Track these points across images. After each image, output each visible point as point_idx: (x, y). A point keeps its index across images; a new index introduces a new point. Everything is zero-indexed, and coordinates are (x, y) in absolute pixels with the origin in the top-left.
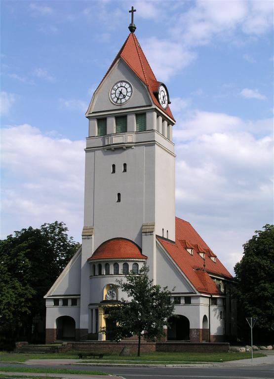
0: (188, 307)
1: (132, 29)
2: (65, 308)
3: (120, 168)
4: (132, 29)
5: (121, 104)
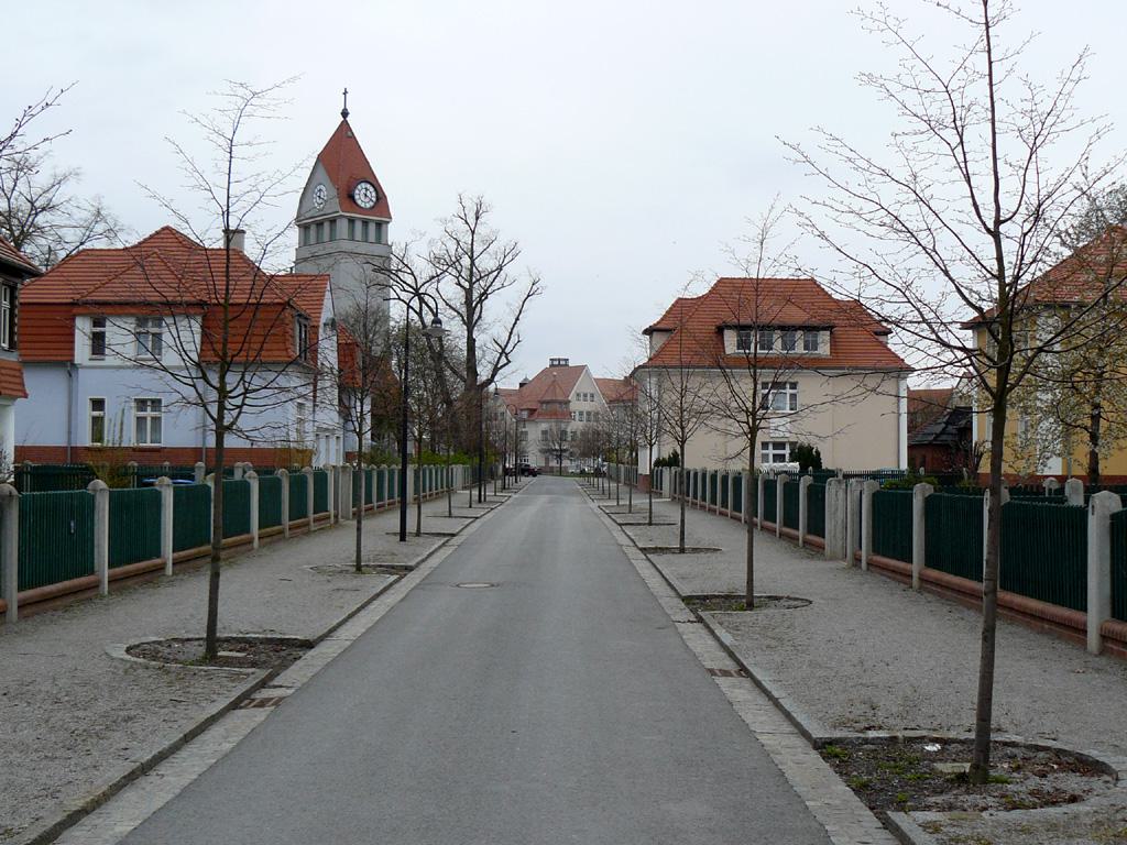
1: (345, 114)
4: (345, 114)
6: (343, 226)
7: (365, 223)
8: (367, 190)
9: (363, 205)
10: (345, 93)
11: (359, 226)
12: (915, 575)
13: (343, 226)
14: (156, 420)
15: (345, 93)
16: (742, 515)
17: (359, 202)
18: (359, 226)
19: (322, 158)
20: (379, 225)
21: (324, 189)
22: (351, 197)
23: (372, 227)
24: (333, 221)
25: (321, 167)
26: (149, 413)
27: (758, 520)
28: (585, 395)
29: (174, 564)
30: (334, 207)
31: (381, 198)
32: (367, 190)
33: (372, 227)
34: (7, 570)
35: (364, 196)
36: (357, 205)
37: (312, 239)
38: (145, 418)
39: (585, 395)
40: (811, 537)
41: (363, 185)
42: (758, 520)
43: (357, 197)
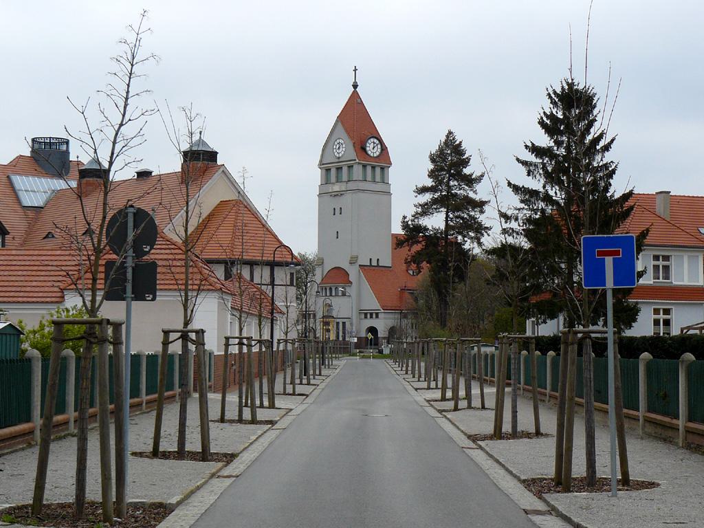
0: (377, 320)
1: (355, 86)
2: (371, 320)
3: (338, 211)
4: (355, 86)
5: (339, 158)
6: (357, 170)
7: (373, 167)
8: (374, 143)
9: (372, 155)
10: (355, 70)
11: (369, 169)
12: (681, 428)
13: (357, 170)
14: (666, 268)
15: (355, 70)
16: (495, 380)
17: (369, 152)
18: (369, 169)
19: (342, 118)
20: (382, 168)
21: (341, 141)
22: (364, 149)
23: (378, 170)
24: (350, 167)
25: (340, 125)
26: (661, 263)
27: (521, 386)
28: (371, 314)
29: (146, 403)
30: (352, 154)
31: (384, 149)
32: (374, 143)
33: (378, 170)
34: (35, 375)
35: (373, 149)
36: (368, 155)
37: (333, 179)
38: (659, 266)
39: (371, 314)
40: (553, 393)
41: (372, 140)
42: (521, 386)
43: (368, 149)
